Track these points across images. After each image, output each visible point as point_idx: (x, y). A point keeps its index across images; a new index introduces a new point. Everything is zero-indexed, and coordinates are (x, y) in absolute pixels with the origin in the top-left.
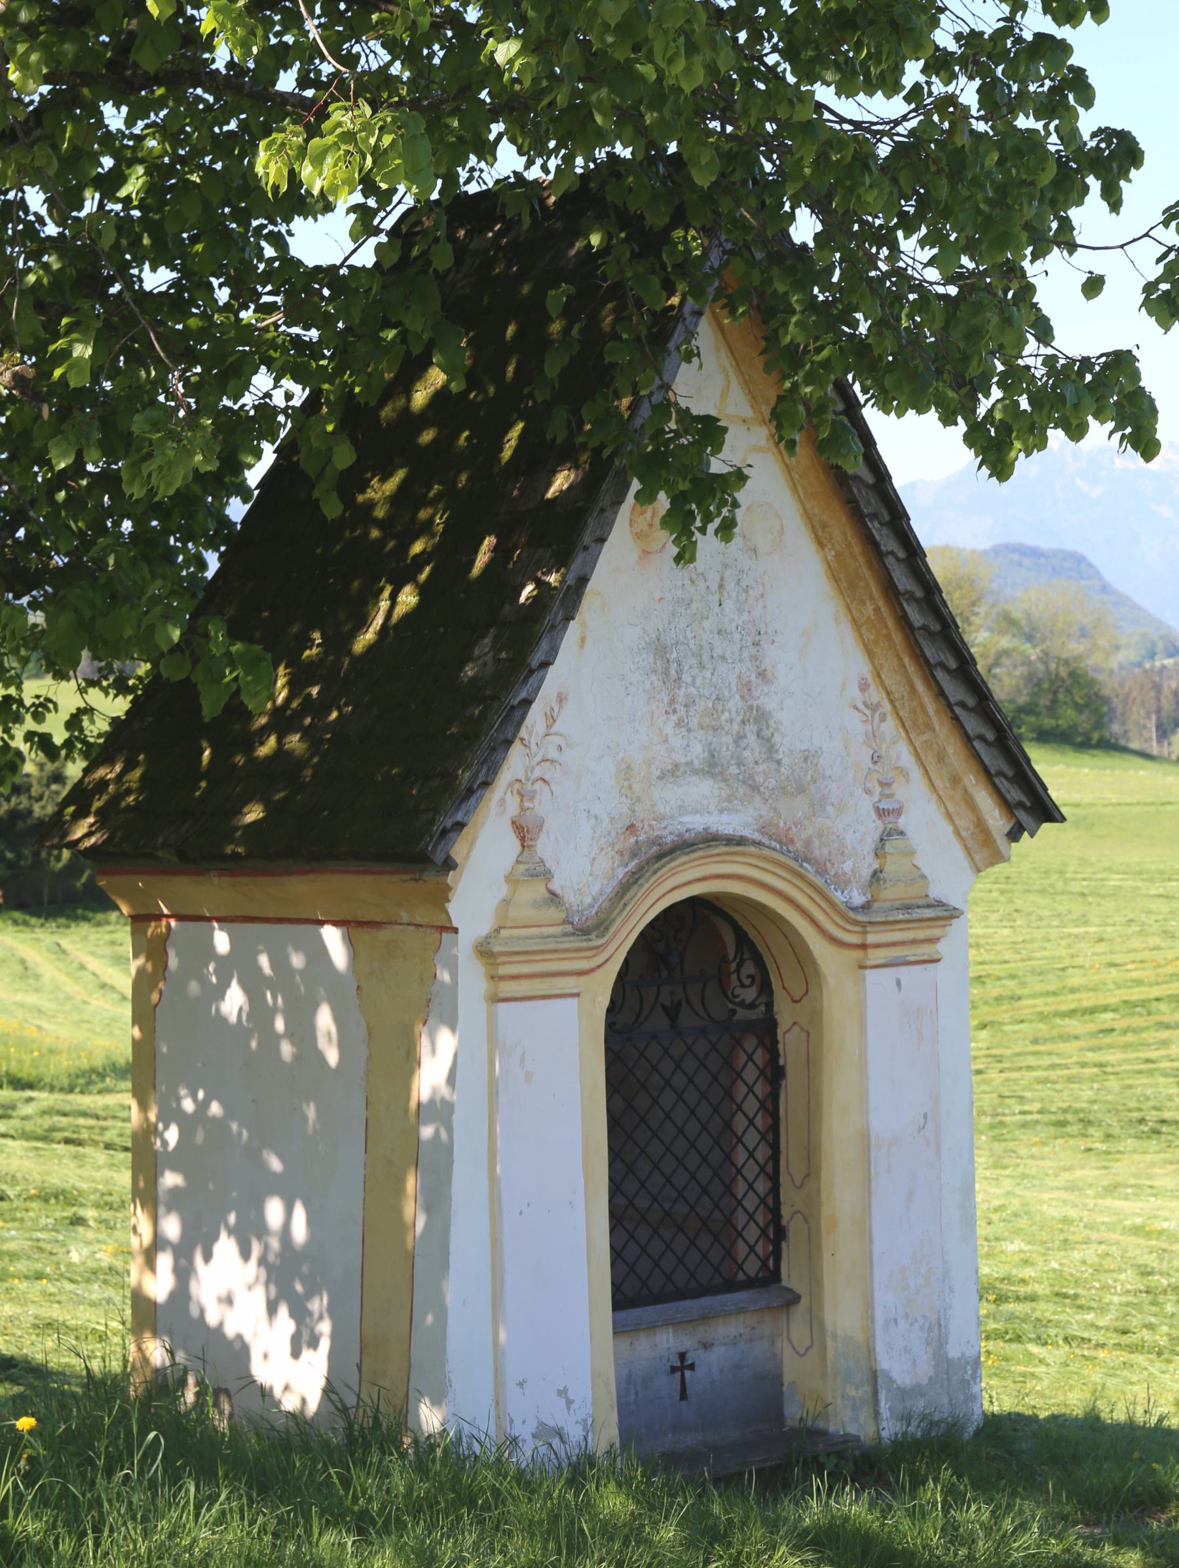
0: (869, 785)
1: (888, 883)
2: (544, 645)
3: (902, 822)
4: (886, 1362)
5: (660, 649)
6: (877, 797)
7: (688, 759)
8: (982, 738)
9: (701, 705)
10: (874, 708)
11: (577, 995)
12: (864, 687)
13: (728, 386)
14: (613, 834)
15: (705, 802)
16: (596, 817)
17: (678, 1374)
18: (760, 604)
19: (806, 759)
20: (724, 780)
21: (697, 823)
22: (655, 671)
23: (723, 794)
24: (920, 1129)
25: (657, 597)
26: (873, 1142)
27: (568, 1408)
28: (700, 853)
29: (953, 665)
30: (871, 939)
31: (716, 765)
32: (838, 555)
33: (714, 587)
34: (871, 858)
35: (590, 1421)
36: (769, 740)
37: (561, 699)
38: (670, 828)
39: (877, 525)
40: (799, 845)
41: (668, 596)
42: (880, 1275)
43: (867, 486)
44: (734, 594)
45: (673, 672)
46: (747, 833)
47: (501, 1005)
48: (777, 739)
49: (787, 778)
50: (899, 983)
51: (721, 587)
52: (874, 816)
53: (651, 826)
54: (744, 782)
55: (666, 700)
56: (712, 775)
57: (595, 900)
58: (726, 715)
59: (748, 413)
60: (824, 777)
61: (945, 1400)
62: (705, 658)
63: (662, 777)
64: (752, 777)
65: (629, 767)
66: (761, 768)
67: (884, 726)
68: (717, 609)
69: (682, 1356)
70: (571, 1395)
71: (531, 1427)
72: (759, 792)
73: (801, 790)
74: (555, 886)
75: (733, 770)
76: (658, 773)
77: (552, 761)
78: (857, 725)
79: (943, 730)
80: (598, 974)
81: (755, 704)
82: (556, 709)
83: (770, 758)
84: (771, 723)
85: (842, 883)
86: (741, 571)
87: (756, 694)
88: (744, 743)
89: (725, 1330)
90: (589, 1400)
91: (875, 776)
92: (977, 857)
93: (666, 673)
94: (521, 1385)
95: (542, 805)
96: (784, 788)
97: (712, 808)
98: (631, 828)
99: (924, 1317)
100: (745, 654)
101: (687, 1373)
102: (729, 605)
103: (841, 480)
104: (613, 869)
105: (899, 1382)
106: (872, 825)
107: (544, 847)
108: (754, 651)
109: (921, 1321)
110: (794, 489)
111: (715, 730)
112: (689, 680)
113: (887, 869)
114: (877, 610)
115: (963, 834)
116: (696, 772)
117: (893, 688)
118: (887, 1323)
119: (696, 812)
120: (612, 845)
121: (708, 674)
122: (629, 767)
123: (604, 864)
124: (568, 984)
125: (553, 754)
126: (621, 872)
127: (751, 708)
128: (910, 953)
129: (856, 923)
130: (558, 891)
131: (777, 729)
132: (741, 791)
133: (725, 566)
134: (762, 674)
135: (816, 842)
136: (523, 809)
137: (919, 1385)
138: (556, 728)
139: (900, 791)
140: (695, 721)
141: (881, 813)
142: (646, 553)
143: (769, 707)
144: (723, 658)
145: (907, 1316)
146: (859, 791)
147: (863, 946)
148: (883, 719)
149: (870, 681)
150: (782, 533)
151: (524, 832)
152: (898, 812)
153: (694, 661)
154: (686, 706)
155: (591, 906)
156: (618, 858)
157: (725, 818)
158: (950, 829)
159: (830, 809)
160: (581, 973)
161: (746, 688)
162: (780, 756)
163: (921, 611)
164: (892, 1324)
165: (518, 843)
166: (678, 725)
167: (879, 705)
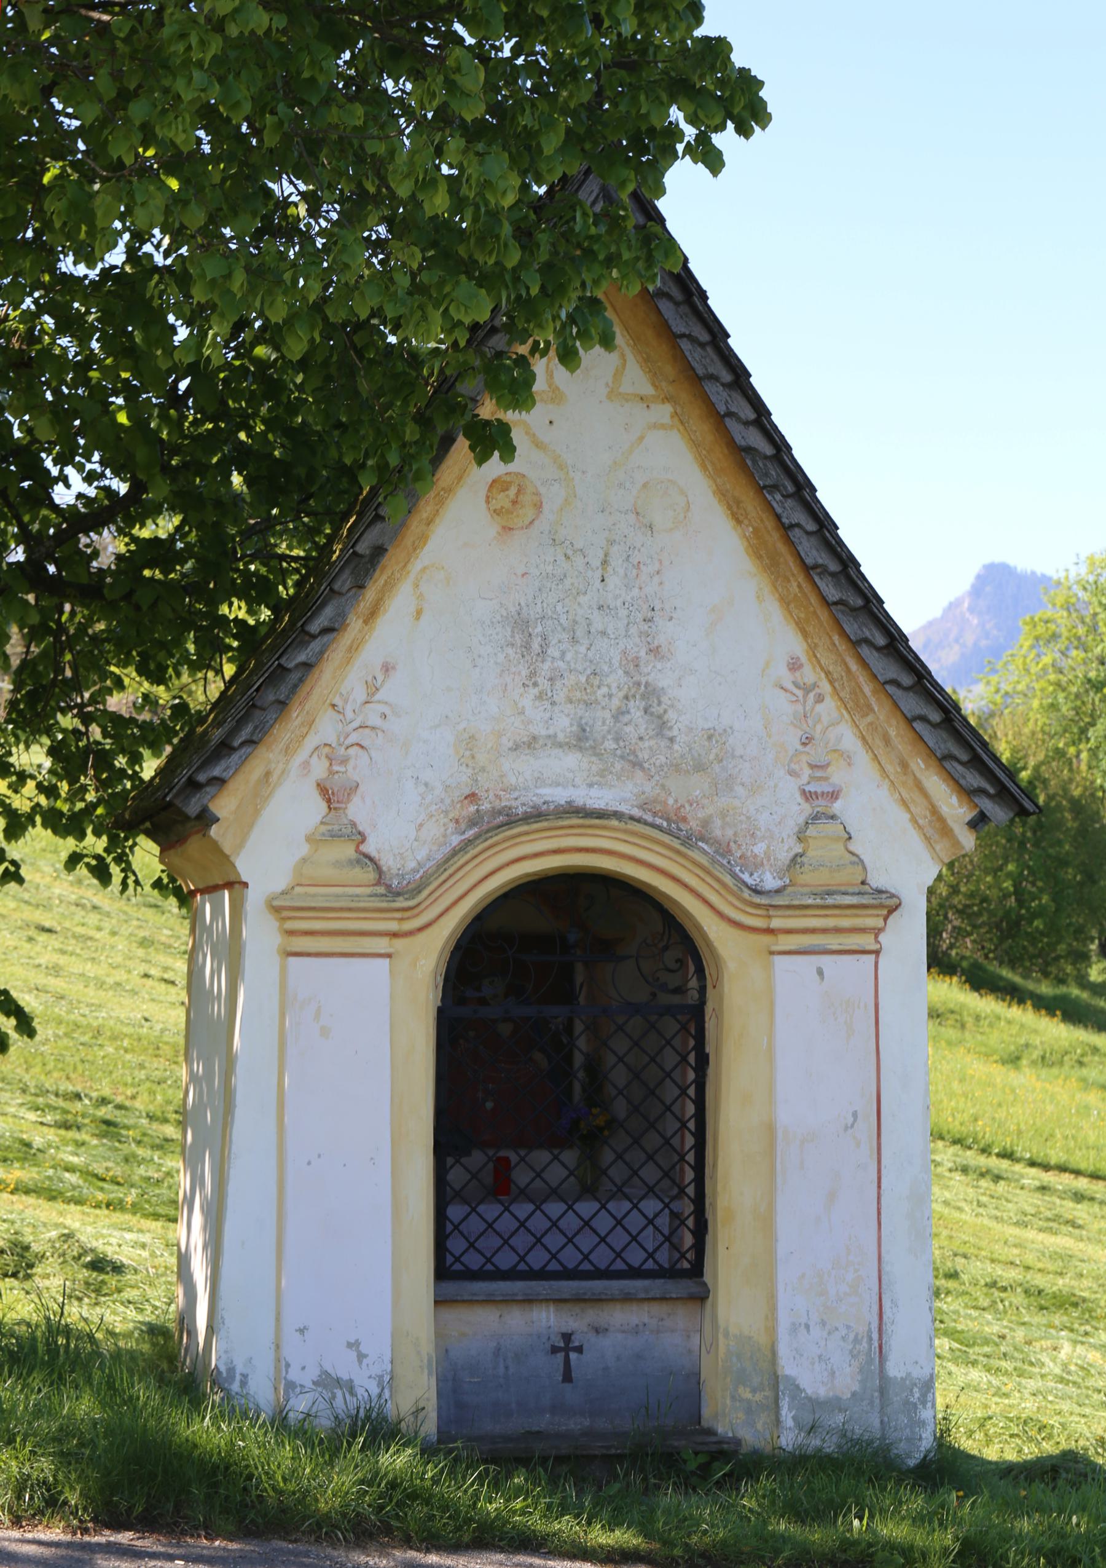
0: (793, 766)
1: (806, 868)
2: (328, 611)
3: (837, 807)
4: (788, 1367)
5: (521, 624)
6: (805, 778)
7: (551, 732)
8: (923, 719)
9: (571, 680)
10: (807, 689)
11: (389, 956)
12: (794, 666)
14: (448, 801)
16: (426, 785)
17: (560, 1356)
18: (656, 579)
19: (710, 738)
20: (598, 755)
21: (559, 796)
23: (594, 768)
24: (846, 1128)
25: (520, 572)
26: (780, 1134)
27: (360, 1362)
28: (545, 824)
29: (881, 641)
30: (776, 923)
31: (587, 739)
32: (756, 531)
33: (596, 563)
35: (387, 1378)
37: (387, 668)
38: (523, 799)
39: (778, 497)
40: (693, 824)
42: (785, 1275)
43: (766, 457)
44: (621, 572)
46: (623, 808)
47: (292, 959)
48: (671, 715)
49: (682, 756)
50: (820, 972)
51: (605, 563)
52: (799, 799)
54: (622, 757)
58: (604, 690)
59: (648, 390)
60: (733, 757)
61: (876, 1423)
62: (580, 633)
63: (516, 748)
65: (472, 737)
66: (647, 744)
67: (819, 708)
70: (363, 1349)
71: (313, 1373)
72: (642, 768)
73: (700, 767)
74: (370, 848)
75: (610, 745)
76: (510, 744)
77: (373, 728)
78: (783, 705)
79: (881, 711)
82: (380, 678)
83: (660, 734)
85: (755, 865)
88: (626, 718)
89: (620, 1316)
90: (387, 1357)
92: (938, 847)
93: (527, 646)
94: (302, 1331)
95: (358, 768)
96: (677, 765)
98: (472, 797)
99: (848, 1327)
101: (573, 1356)
102: (613, 581)
103: (742, 453)
104: (445, 836)
105: (809, 1392)
106: (796, 808)
107: (357, 811)
108: (645, 627)
110: (703, 467)
111: (588, 704)
112: (557, 654)
113: (810, 853)
114: (799, 586)
115: (921, 822)
116: (560, 745)
117: (831, 668)
118: (794, 1329)
120: (446, 812)
121: (583, 649)
123: (433, 830)
124: (381, 945)
125: (374, 720)
126: (455, 840)
127: (639, 684)
128: (833, 942)
129: (758, 906)
130: (374, 854)
131: (672, 706)
132: (618, 766)
133: (612, 543)
134: (655, 651)
135: (718, 822)
136: (332, 773)
137: (838, 1399)
138: (378, 696)
139: (838, 776)
141: (808, 796)
144: (604, 633)
145: (823, 1323)
147: (770, 931)
148: (820, 699)
149: (804, 659)
150: (688, 507)
152: (834, 796)
153: (565, 636)
155: (415, 871)
156: (452, 825)
157: (595, 792)
158: (907, 816)
159: (740, 790)
160: (395, 935)
162: (675, 732)
163: (837, 585)
165: (323, 805)
166: (540, 697)
167: (815, 685)
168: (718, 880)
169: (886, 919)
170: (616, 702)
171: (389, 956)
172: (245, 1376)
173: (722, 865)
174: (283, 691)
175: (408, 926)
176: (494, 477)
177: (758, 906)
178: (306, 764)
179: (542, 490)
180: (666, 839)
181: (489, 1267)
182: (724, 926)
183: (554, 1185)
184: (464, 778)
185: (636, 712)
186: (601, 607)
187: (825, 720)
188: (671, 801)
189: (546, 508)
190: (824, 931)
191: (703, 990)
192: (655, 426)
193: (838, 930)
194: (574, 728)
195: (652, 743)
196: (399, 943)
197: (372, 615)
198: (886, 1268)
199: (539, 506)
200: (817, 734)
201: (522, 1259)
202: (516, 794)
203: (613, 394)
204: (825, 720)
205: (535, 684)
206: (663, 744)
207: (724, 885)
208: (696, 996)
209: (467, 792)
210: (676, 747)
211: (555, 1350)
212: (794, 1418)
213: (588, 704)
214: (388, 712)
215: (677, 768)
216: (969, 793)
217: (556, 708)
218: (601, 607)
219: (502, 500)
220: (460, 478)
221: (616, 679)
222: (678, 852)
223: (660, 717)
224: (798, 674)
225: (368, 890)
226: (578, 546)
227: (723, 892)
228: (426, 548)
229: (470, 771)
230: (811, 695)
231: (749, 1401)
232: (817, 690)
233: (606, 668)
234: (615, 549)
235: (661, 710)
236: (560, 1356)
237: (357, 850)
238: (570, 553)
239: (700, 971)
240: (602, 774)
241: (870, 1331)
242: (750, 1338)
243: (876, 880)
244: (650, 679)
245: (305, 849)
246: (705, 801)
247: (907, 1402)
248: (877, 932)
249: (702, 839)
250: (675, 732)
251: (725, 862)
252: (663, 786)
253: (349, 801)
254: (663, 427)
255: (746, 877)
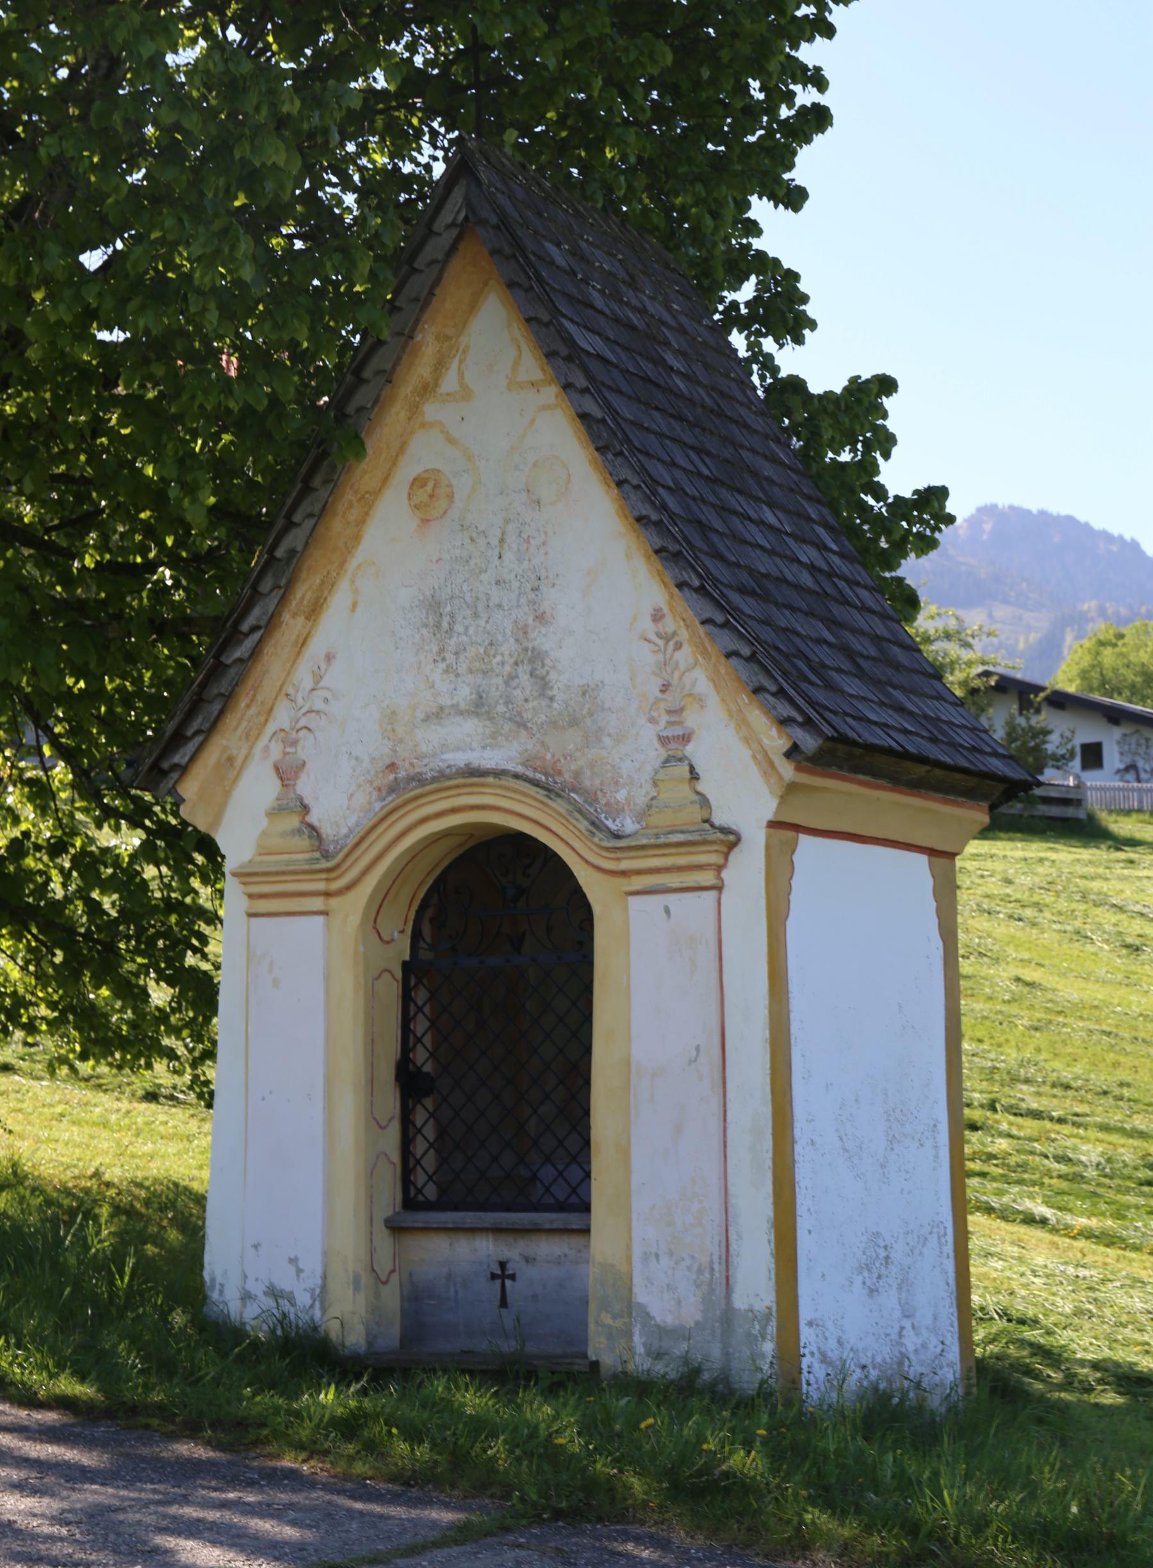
0: (654, 714)
4: (641, 1296)
5: (433, 605)
6: (662, 724)
9: (472, 651)
10: (667, 638)
12: (657, 617)
13: (520, 356)
14: (373, 772)
15: (468, 740)
16: (357, 758)
17: (498, 1282)
18: (542, 551)
19: (584, 694)
20: (491, 719)
21: (459, 759)
22: (426, 626)
23: (488, 731)
25: (434, 559)
33: (495, 542)
34: (648, 786)
35: (318, 1291)
36: (543, 678)
37: (329, 658)
38: (432, 765)
40: (567, 776)
41: (446, 556)
42: (639, 1205)
44: (514, 546)
45: (445, 625)
48: (553, 676)
49: (560, 714)
50: (667, 911)
51: (502, 541)
52: (657, 745)
53: (412, 765)
54: (510, 719)
55: (435, 649)
56: (477, 714)
57: (351, 831)
58: (499, 658)
59: (538, 375)
61: (716, 1351)
62: (481, 608)
63: (426, 719)
64: (520, 714)
65: (394, 713)
66: (531, 705)
67: (678, 655)
68: (496, 561)
69: (503, 1265)
73: (574, 722)
74: (313, 818)
75: (501, 708)
76: (422, 716)
77: (318, 712)
78: (646, 656)
80: (351, 895)
81: (530, 645)
82: (323, 667)
83: (542, 695)
84: (548, 662)
85: (615, 811)
86: (524, 524)
87: (532, 635)
88: (514, 683)
90: (319, 1271)
91: (662, 705)
93: (438, 626)
94: (256, 1247)
95: (306, 749)
97: (474, 744)
98: (392, 767)
99: (693, 1257)
100: (523, 600)
101: (508, 1283)
102: (508, 556)
104: (370, 803)
105: (658, 1319)
107: (304, 787)
108: (532, 596)
109: (688, 1262)
111: (485, 673)
116: (461, 713)
118: (646, 1257)
119: (458, 749)
120: (371, 782)
121: (482, 623)
122: (394, 713)
123: (361, 799)
124: (317, 903)
125: (319, 705)
127: (526, 649)
128: (674, 880)
130: (316, 823)
131: (553, 667)
132: (507, 727)
133: (507, 521)
134: (540, 618)
135: (588, 773)
136: (286, 754)
138: (321, 684)
139: (691, 719)
140: (464, 666)
141: (664, 741)
142: (425, 521)
143: (546, 647)
144: (500, 606)
145: (671, 1253)
146: (642, 720)
148: (678, 646)
149: (666, 610)
151: (287, 774)
152: (686, 738)
153: (468, 612)
154: (456, 653)
155: (347, 836)
156: (375, 794)
157: (488, 754)
159: (607, 741)
160: (327, 894)
161: (523, 631)
162: (555, 692)
164: (653, 1258)
165: (279, 782)
167: (675, 633)
169: (726, 856)
170: (508, 668)
171: (325, 913)
172: (222, 1285)
174: (224, 686)
175: (336, 885)
176: (414, 474)
177: (607, 849)
178: (266, 748)
179: (454, 482)
182: (591, 870)
184: (387, 750)
185: (524, 678)
186: (498, 583)
187: (682, 667)
188: (549, 756)
189: (457, 497)
190: (668, 870)
192: (544, 408)
193: (680, 869)
194: (474, 696)
195: (535, 703)
196: (334, 902)
197: (315, 611)
198: (732, 1200)
199: (451, 497)
200: (675, 682)
202: (426, 761)
203: (513, 384)
204: (682, 667)
205: (444, 659)
206: (544, 703)
209: (388, 762)
210: (555, 705)
211: (494, 1276)
212: (644, 1344)
213: (485, 673)
214: (329, 697)
215: (554, 724)
216: (784, 722)
217: (459, 680)
218: (498, 583)
219: (422, 496)
220: (385, 480)
221: (509, 647)
223: (543, 678)
224: (660, 625)
225: (307, 856)
226: (481, 529)
228: (361, 547)
229: (390, 744)
230: (671, 644)
231: (610, 1327)
232: (676, 638)
233: (500, 638)
234: (510, 527)
235: (544, 672)
236: (498, 1282)
237: (303, 822)
238: (474, 535)
240: (493, 736)
241: (712, 1262)
242: (613, 1266)
243: (720, 818)
244: (536, 643)
245: (265, 822)
246: (578, 754)
247: (749, 1334)
248: (719, 868)
249: (574, 790)
250: (555, 692)
252: (543, 743)
253: (297, 778)
254: (549, 407)
255: (609, 823)
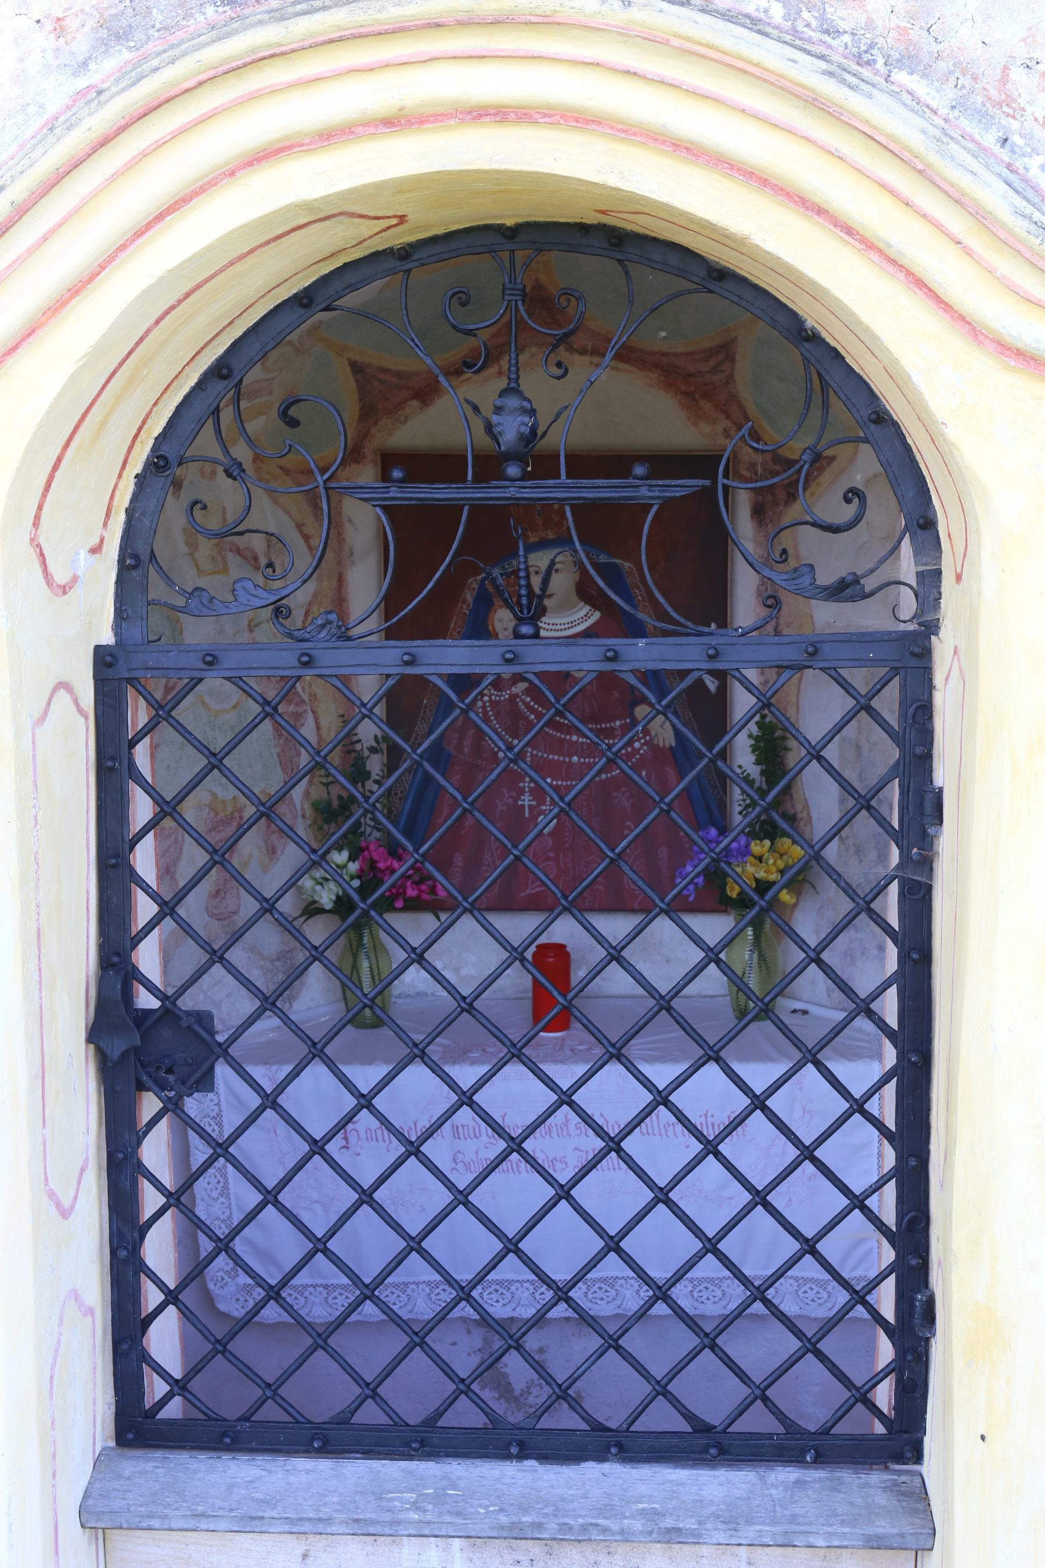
168: (959, 200)
173: (981, 151)
180: (772, 55)
181: (271, 1412)
183: (712, 1069)
191: (930, 582)
201: (371, 1391)
207: (980, 216)
208: (908, 604)
222: (815, 103)
227: (976, 241)
239: (924, 525)
249: (909, 60)
251: (990, 140)
